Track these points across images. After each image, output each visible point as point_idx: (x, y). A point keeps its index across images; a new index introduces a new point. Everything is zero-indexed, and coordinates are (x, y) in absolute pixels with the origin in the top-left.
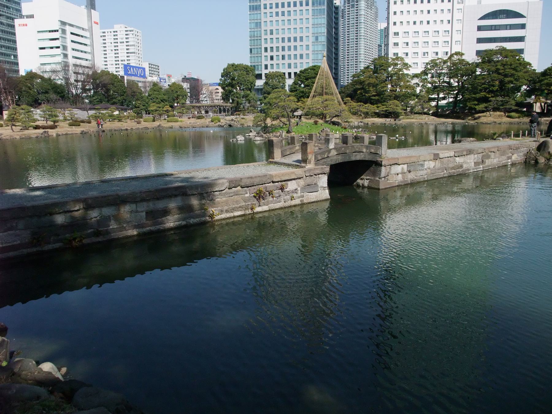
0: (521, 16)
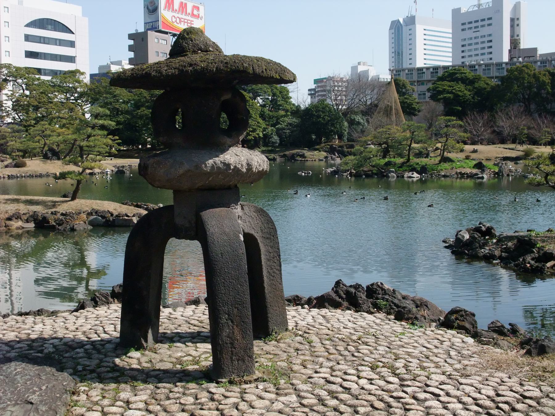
0: (67, 30)
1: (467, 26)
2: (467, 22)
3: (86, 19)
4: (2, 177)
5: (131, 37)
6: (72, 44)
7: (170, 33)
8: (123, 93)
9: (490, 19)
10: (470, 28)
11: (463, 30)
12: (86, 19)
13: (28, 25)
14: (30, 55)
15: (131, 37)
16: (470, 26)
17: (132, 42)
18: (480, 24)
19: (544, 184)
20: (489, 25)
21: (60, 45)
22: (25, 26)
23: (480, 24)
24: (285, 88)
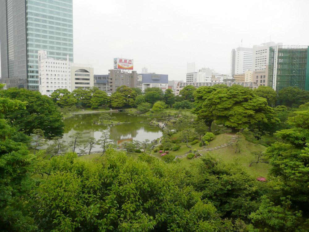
0: (88, 72)
11: (257, 54)
15: (109, 71)
18: (263, 51)
23: (263, 51)
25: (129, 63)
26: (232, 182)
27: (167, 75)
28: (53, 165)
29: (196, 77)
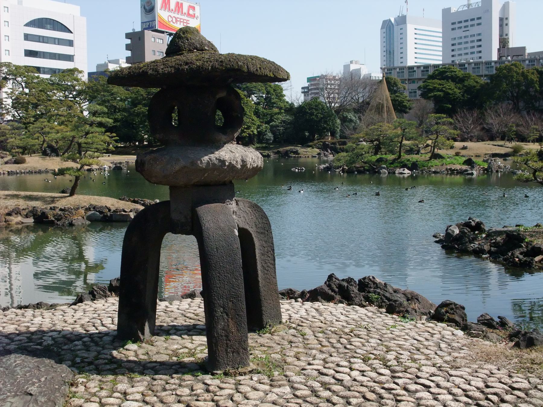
0: (66, 29)
1: (457, 26)
2: (457, 21)
3: (84, 19)
4: (2, 173)
5: (128, 36)
6: (70, 43)
7: (167, 32)
8: (120, 91)
9: (479, 18)
10: (460, 28)
11: (453, 29)
12: (84, 19)
13: (27, 25)
14: (30, 53)
15: (128, 36)
16: (460, 25)
17: (129, 41)
18: (470, 23)
19: (532, 180)
20: (479, 24)
21: (58, 44)
22: (25, 26)
23: (470, 23)
24: (279, 86)
25: (189, 15)
26: (496, 352)
27: (126, 57)
28: (305, 337)
29: (59, 72)
